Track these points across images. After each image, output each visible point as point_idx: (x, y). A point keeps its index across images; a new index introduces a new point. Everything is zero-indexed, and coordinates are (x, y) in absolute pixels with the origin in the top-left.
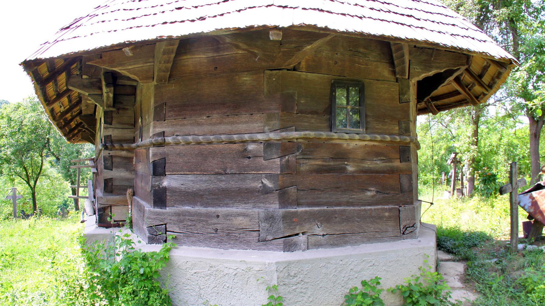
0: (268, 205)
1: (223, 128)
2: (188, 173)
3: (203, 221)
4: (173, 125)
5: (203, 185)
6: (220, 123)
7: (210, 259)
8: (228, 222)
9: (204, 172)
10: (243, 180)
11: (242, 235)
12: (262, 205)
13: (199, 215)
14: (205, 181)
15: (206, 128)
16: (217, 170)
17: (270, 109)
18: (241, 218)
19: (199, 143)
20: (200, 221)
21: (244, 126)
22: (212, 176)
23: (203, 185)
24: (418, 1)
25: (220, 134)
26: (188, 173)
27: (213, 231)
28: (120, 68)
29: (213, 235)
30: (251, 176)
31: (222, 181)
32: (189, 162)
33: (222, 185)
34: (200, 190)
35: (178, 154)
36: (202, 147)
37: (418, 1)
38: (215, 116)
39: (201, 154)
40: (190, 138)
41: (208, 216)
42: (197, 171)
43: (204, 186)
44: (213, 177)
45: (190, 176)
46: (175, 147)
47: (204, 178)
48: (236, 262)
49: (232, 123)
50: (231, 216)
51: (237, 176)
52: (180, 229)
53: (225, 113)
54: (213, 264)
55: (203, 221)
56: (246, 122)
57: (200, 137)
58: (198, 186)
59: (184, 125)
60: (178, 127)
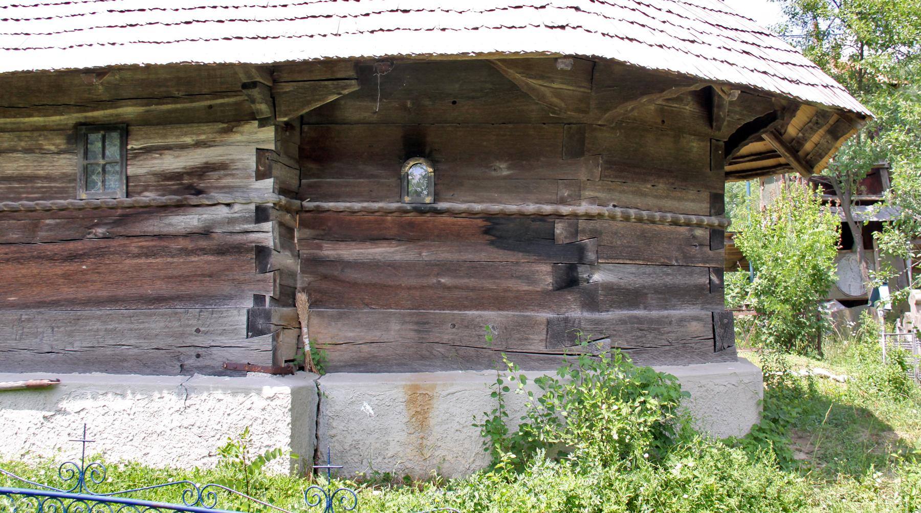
0: (715, 307)
1: (669, 203)
2: (628, 262)
3: (655, 329)
4: (610, 190)
5: (648, 280)
6: (666, 197)
7: (699, 377)
8: (682, 329)
9: (648, 261)
10: (691, 274)
11: (698, 346)
12: (708, 306)
13: (651, 321)
14: (650, 274)
15: (650, 201)
16: (662, 260)
17: (715, 188)
18: (694, 323)
19: (640, 220)
20: (650, 330)
21: (692, 204)
22: (657, 269)
23: (648, 280)
24: (602, 3)
25: (666, 212)
26: (628, 262)
27: (667, 343)
28: (540, 82)
29: (667, 348)
30: (698, 270)
31: (668, 274)
32: (630, 247)
33: (668, 280)
34: (644, 287)
35: (616, 234)
36: (645, 226)
37: (602, 3)
38: (662, 186)
39: (643, 235)
40: (632, 212)
41: (659, 321)
42: (639, 259)
43: (648, 281)
44: (658, 269)
45: (627, 266)
46: (611, 222)
47: (648, 270)
48: (725, 375)
49: (680, 199)
50: (685, 321)
51: (684, 268)
52: (628, 342)
53: (673, 184)
54: (703, 382)
55: (655, 329)
56: (693, 201)
57: (644, 213)
58: (641, 281)
59: (623, 192)
60: (617, 194)
